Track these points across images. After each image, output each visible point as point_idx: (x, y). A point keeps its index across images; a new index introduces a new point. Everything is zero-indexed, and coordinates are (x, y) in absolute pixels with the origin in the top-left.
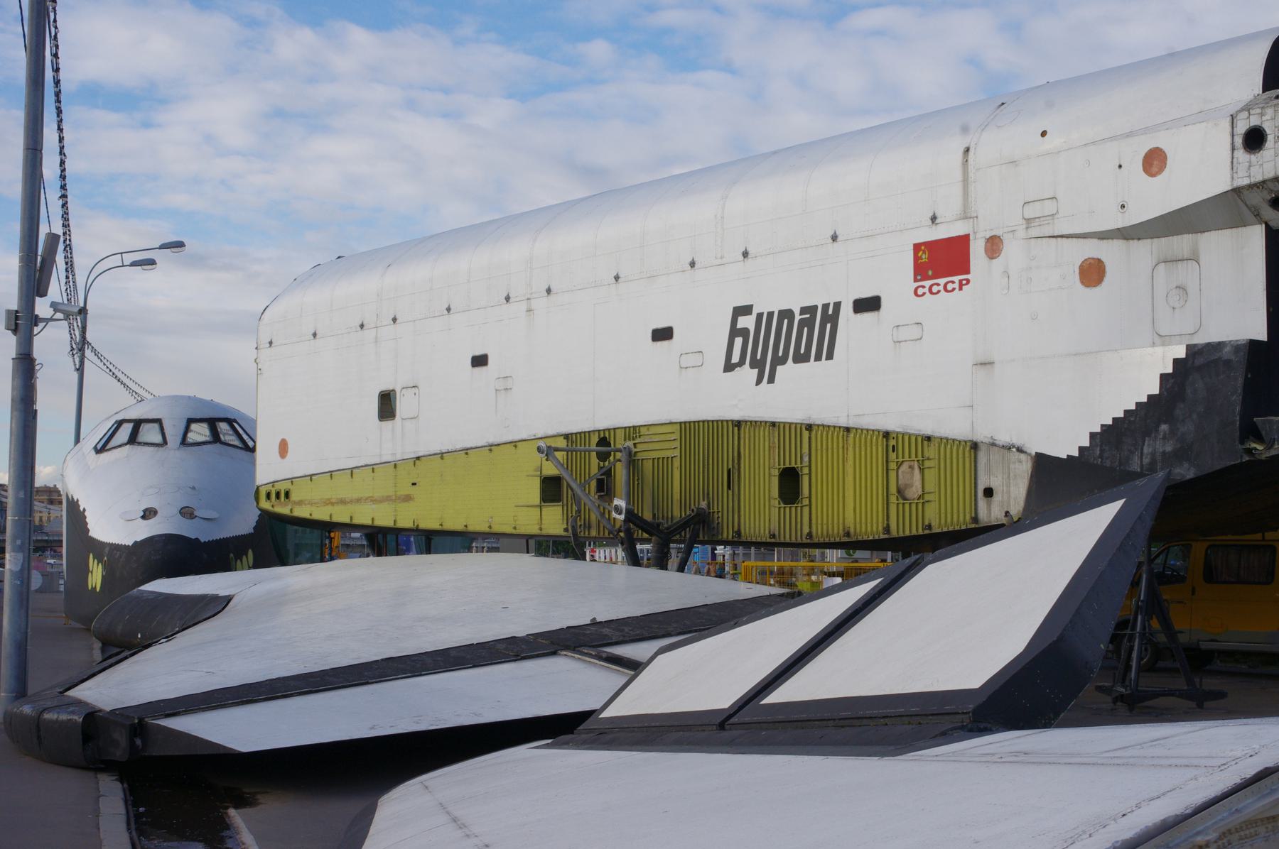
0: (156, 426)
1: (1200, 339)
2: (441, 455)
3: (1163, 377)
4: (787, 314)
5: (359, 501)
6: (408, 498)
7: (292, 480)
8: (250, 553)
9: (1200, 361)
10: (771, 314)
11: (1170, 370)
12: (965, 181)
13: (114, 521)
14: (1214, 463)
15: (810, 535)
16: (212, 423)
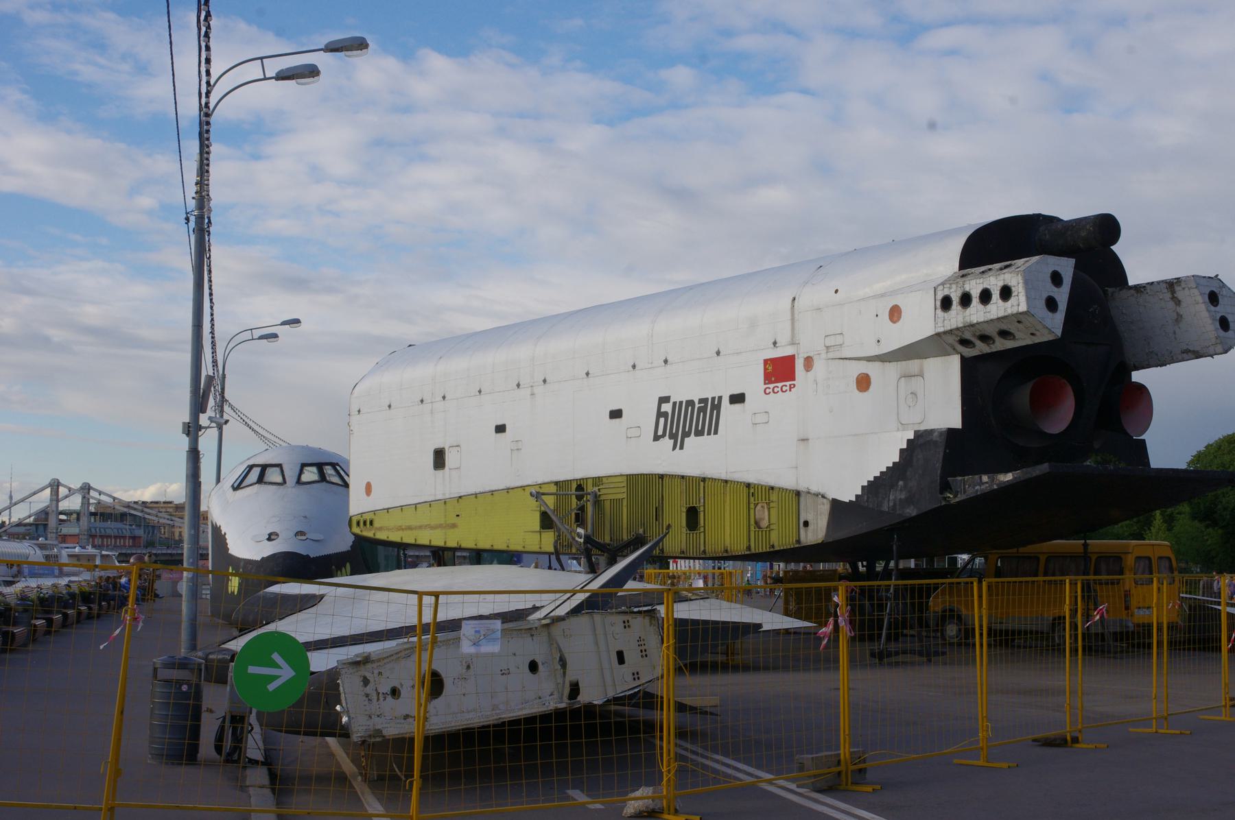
0: (278, 469)
1: (922, 428)
2: (476, 495)
3: (901, 450)
4: (690, 403)
5: (420, 527)
6: (454, 526)
7: (374, 512)
8: (348, 565)
9: (921, 441)
10: (681, 403)
11: (905, 446)
12: (793, 319)
14: (927, 506)
15: (704, 552)
16: (320, 466)
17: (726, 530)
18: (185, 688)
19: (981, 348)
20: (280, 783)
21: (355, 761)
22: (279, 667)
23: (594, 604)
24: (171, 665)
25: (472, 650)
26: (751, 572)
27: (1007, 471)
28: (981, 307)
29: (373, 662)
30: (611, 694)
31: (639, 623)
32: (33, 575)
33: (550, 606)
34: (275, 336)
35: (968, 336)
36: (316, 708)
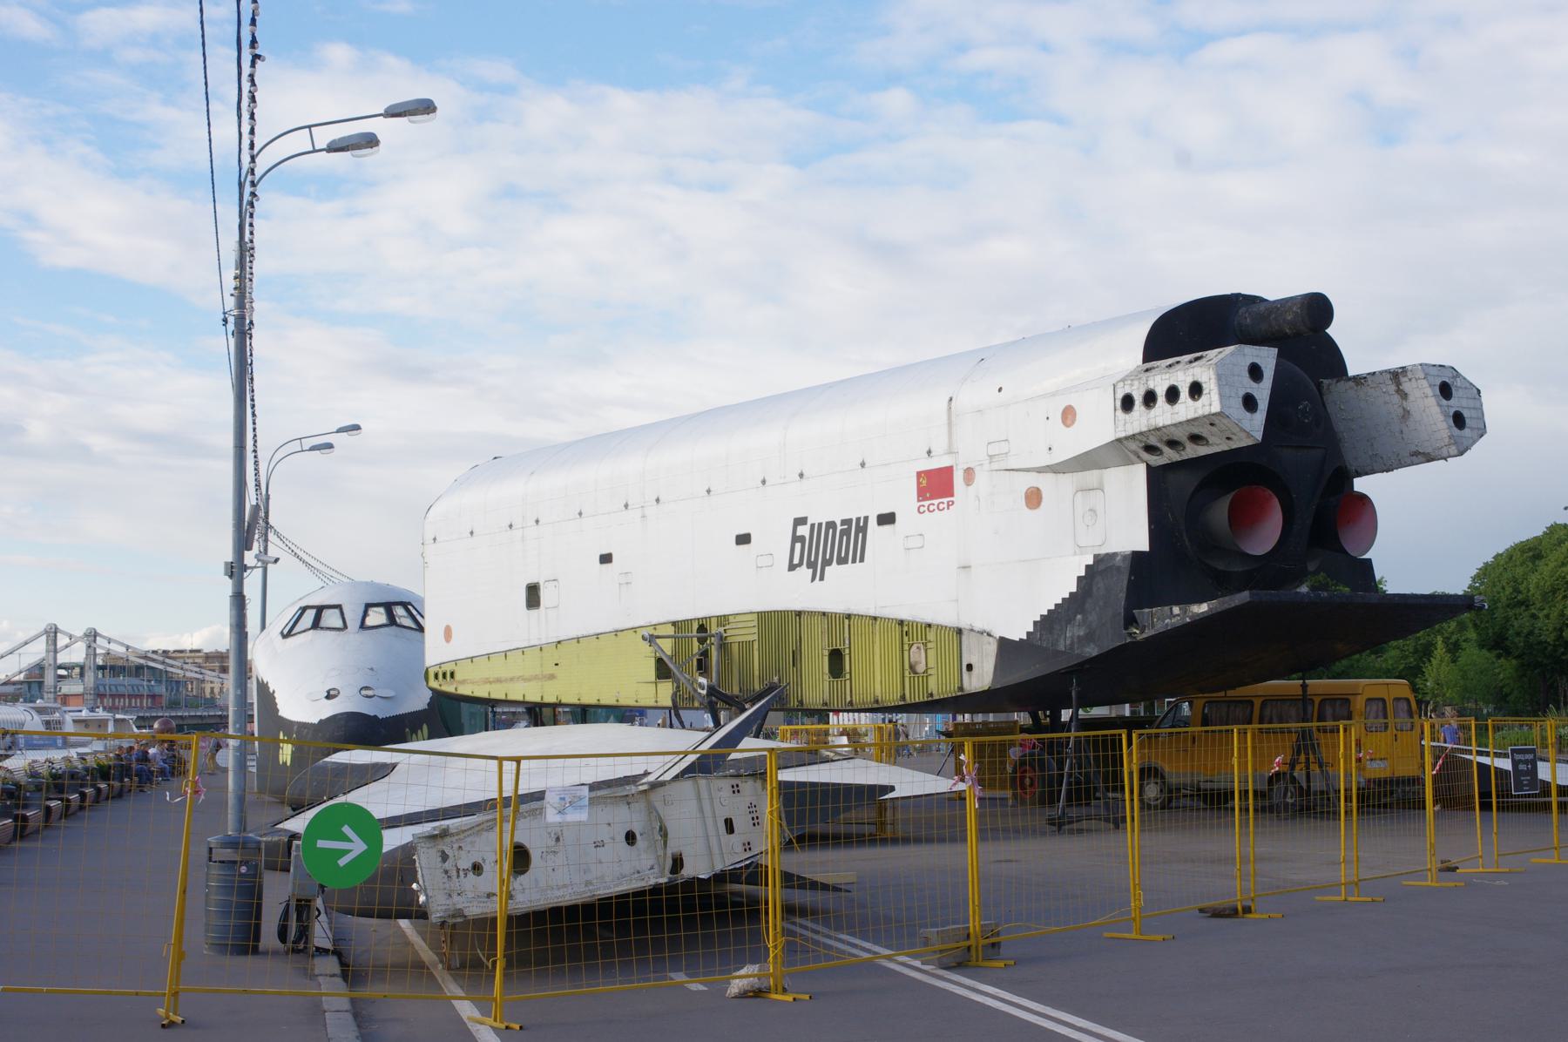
0: (337, 611)
1: (1103, 551)
2: (578, 639)
3: (1079, 578)
4: (831, 525)
5: (512, 679)
6: (552, 677)
9: (1102, 567)
10: (820, 525)
12: (950, 424)
13: (302, 703)
14: (1111, 643)
15: (851, 703)
16: (388, 607)
17: (876, 675)
18: (244, 869)
19: (1170, 456)
20: (350, 973)
21: (434, 947)
22: (350, 840)
23: (704, 766)
24: (232, 844)
25: (558, 818)
26: (925, 727)
27: (1201, 602)
28: (1167, 406)
29: (452, 835)
30: (719, 867)
31: (748, 786)
32: (32, 746)
33: (657, 769)
34: (330, 446)
35: (1153, 441)
36: (389, 888)
